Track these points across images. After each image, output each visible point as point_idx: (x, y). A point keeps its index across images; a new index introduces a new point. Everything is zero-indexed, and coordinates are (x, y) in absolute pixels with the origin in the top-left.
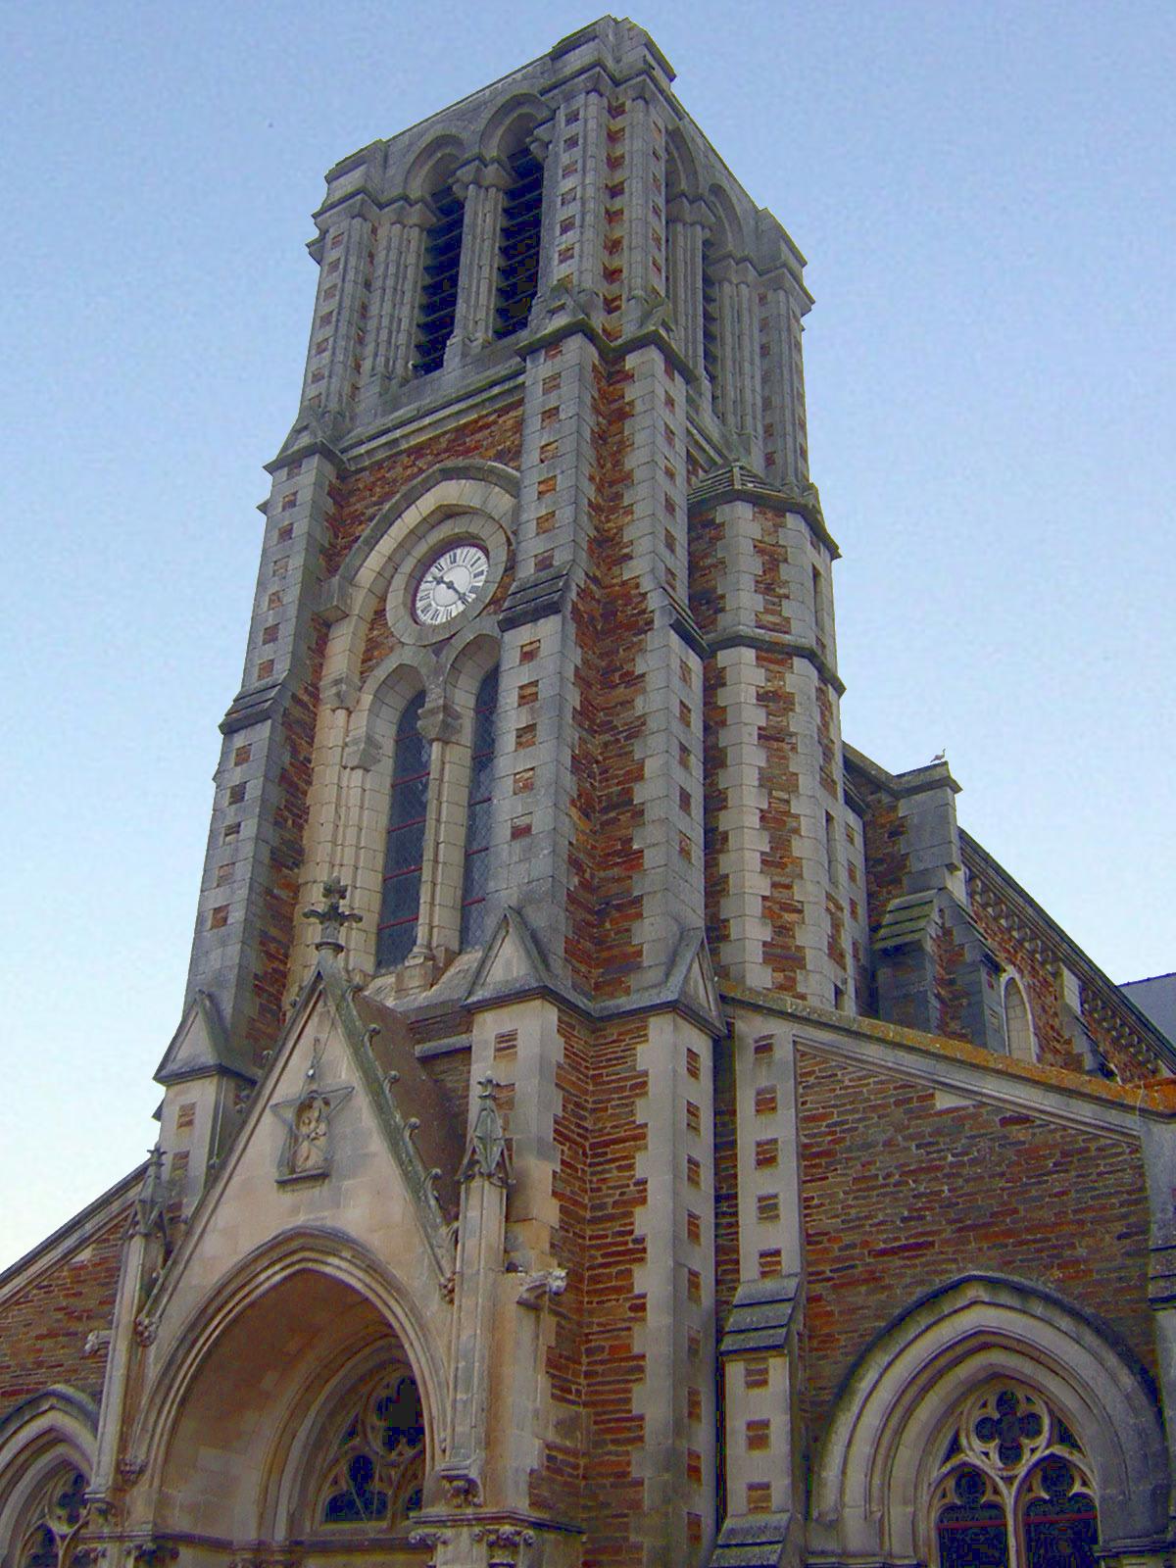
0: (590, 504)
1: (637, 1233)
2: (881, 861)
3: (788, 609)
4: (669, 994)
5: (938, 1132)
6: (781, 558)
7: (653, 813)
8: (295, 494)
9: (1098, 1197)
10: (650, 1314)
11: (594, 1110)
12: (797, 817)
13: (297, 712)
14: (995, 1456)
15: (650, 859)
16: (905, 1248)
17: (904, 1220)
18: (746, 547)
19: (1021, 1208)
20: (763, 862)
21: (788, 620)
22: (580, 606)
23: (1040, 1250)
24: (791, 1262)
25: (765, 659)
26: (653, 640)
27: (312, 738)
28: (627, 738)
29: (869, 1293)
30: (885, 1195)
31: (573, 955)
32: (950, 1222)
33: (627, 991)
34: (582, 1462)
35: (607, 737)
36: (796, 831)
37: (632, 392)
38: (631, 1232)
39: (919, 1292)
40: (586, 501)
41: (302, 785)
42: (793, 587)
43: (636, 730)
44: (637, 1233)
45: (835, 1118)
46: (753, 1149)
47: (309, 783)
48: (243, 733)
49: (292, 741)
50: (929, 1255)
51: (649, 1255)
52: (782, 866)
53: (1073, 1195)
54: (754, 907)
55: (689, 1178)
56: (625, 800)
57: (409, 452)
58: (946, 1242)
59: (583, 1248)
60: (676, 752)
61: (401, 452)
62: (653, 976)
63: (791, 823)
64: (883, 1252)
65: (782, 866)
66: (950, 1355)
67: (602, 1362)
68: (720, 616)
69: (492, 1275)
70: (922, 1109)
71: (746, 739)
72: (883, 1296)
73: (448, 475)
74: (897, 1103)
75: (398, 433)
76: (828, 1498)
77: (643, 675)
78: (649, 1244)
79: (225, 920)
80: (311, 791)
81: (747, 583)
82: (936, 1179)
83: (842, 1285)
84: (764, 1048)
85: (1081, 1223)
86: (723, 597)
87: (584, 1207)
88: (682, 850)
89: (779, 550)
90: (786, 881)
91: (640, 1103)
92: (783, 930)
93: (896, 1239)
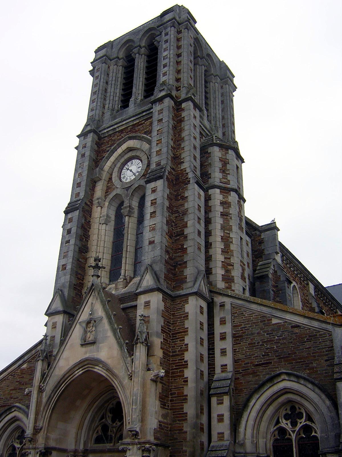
1: (185, 359)
3: (229, 177)
4: (195, 290)
5: (273, 330)
8: (86, 144)
9: (319, 349)
11: (173, 324)
12: (232, 238)
13: (87, 208)
14: (289, 424)
15: (189, 250)
16: (263, 364)
17: (263, 356)
21: (229, 181)
22: (169, 177)
24: (230, 368)
25: (222, 192)
26: (190, 186)
27: (91, 215)
28: (182, 215)
30: (257, 348)
32: (276, 356)
33: (182, 289)
35: (177, 215)
36: (232, 242)
37: (184, 114)
38: (184, 359)
44: (185, 359)
45: (243, 326)
47: (90, 228)
48: (71, 214)
49: (85, 216)
53: (312, 348)
54: (219, 264)
57: (119, 132)
59: (170, 364)
61: (117, 132)
62: (190, 284)
64: (257, 365)
67: (175, 397)
68: (209, 180)
71: (217, 215)
72: (257, 378)
73: (130, 138)
74: (261, 322)
75: (116, 126)
76: (241, 436)
79: (65, 268)
81: (217, 170)
83: (245, 375)
84: (222, 306)
85: (314, 356)
87: (170, 352)
88: (198, 248)
89: (227, 160)
90: (229, 257)
92: (228, 271)
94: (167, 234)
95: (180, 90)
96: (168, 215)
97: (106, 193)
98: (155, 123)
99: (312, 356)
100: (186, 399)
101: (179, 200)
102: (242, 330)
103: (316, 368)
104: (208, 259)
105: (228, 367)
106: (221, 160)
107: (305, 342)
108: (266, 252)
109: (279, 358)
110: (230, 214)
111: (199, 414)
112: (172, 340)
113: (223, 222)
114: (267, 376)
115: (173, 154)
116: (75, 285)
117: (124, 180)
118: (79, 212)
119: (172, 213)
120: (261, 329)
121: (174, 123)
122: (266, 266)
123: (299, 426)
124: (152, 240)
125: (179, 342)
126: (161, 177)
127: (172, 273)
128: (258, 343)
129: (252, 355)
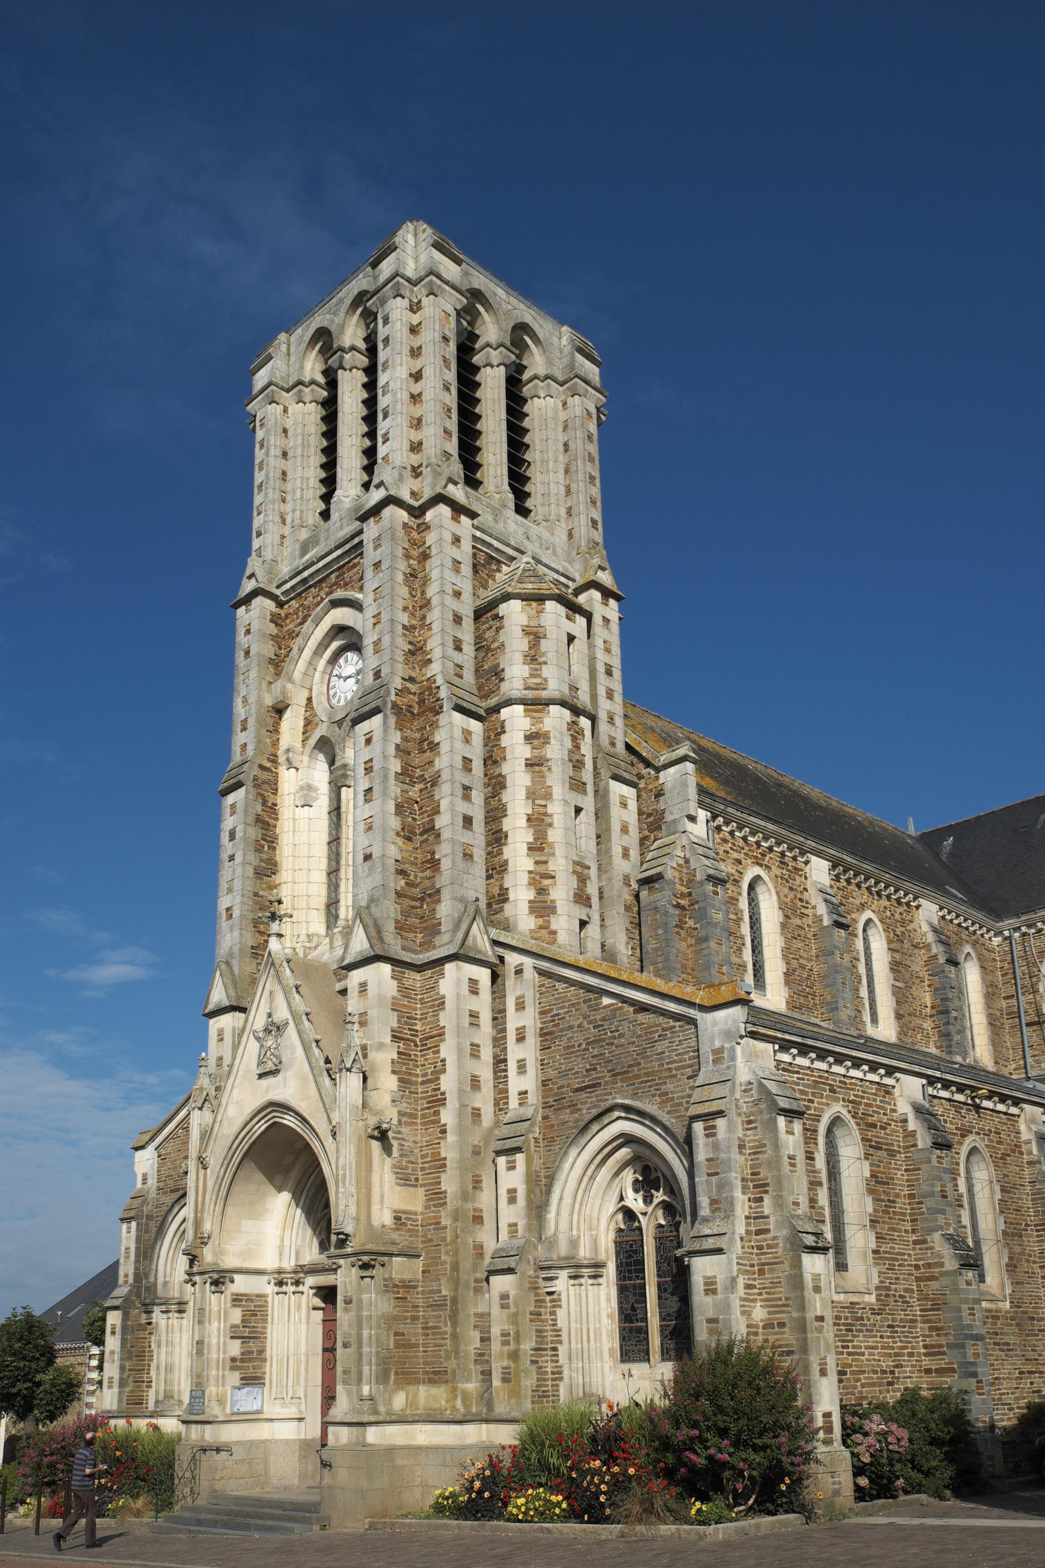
0: (405, 627)
1: (442, 1089)
2: (649, 815)
3: (546, 671)
4: (452, 950)
5: (603, 1019)
6: (541, 635)
7: (445, 835)
8: (249, 625)
9: (679, 1054)
10: (448, 1135)
11: (421, 1019)
12: (551, 815)
13: (264, 776)
14: (640, 1200)
15: (445, 864)
16: (587, 1087)
17: (588, 1071)
18: (518, 632)
19: (642, 1061)
20: (529, 849)
21: (546, 680)
22: (399, 702)
23: (650, 1086)
24: (532, 1098)
25: (531, 710)
26: (443, 719)
27: (277, 790)
28: (432, 786)
29: (572, 1113)
30: (577, 1056)
31: (401, 929)
32: (609, 1071)
33: (434, 948)
34: (420, 1217)
35: (421, 786)
36: (551, 825)
37: (431, 539)
38: (439, 1089)
39: (595, 1112)
40: (400, 627)
41: (272, 821)
42: (549, 655)
43: (435, 782)
44: (442, 1089)
45: (555, 1012)
46: (514, 1033)
47: (277, 819)
48: (232, 794)
49: (262, 796)
50: (599, 1091)
51: (447, 1102)
52: (541, 849)
53: (667, 1054)
54: (524, 879)
55: (471, 1055)
56: (430, 829)
57: (314, 585)
58: (606, 1083)
59: (416, 1100)
60: (459, 792)
61: (310, 587)
62: (446, 938)
63: (548, 820)
64: (577, 1090)
65: (541, 849)
66: (610, 1148)
67: (428, 1162)
68: (502, 684)
69: (355, 1123)
70: (597, 1005)
71: (517, 768)
72: (577, 1115)
73: (336, 604)
74: (585, 1002)
75: (306, 574)
76: (550, 1229)
77: (438, 744)
78: (447, 1095)
79: (231, 915)
80: (279, 824)
81: (518, 657)
82: (601, 1046)
83: (559, 1109)
84: (519, 972)
85: (670, 1070)
86: (503, 670)
87: (417, 1076)
88: (465, 855)
89: (540, 630)
90: (544, 859)
91: (442, 1014)
92: (542, 891)
93: (584, 1082)
94: (398, 834)
95: (421, 473)
96: (399, 790)
97: (304, 733)
98: (369, 573)
99: (666, 1069)
100: (444, 1165)
101: (425, 751)
102: (553, 1021)
103: (672, 1092)
104: (496, 869)
105: (529, 1095)
106: (527, 631)
107: (656, 1042)
108: (669, 818)
109: (613, 1075)
110: (548, 760)
111: (471, 1191)
112: (421, 1051)
113: (533, 781)
114: (594, 1111)
115: (410, 643)
116: (253, 948)
117: (334, 702)
118: (247, 792)
119: (412, 783)
120: (585, 1018)
121: (410, 566)
122: (666, 850)
123: (656, 1201)
124: (368, 851)
125: (432, 1055)
126: (376, 711)
127: (417, 916)
128: (580, 1045)
129: (570, 1070)
